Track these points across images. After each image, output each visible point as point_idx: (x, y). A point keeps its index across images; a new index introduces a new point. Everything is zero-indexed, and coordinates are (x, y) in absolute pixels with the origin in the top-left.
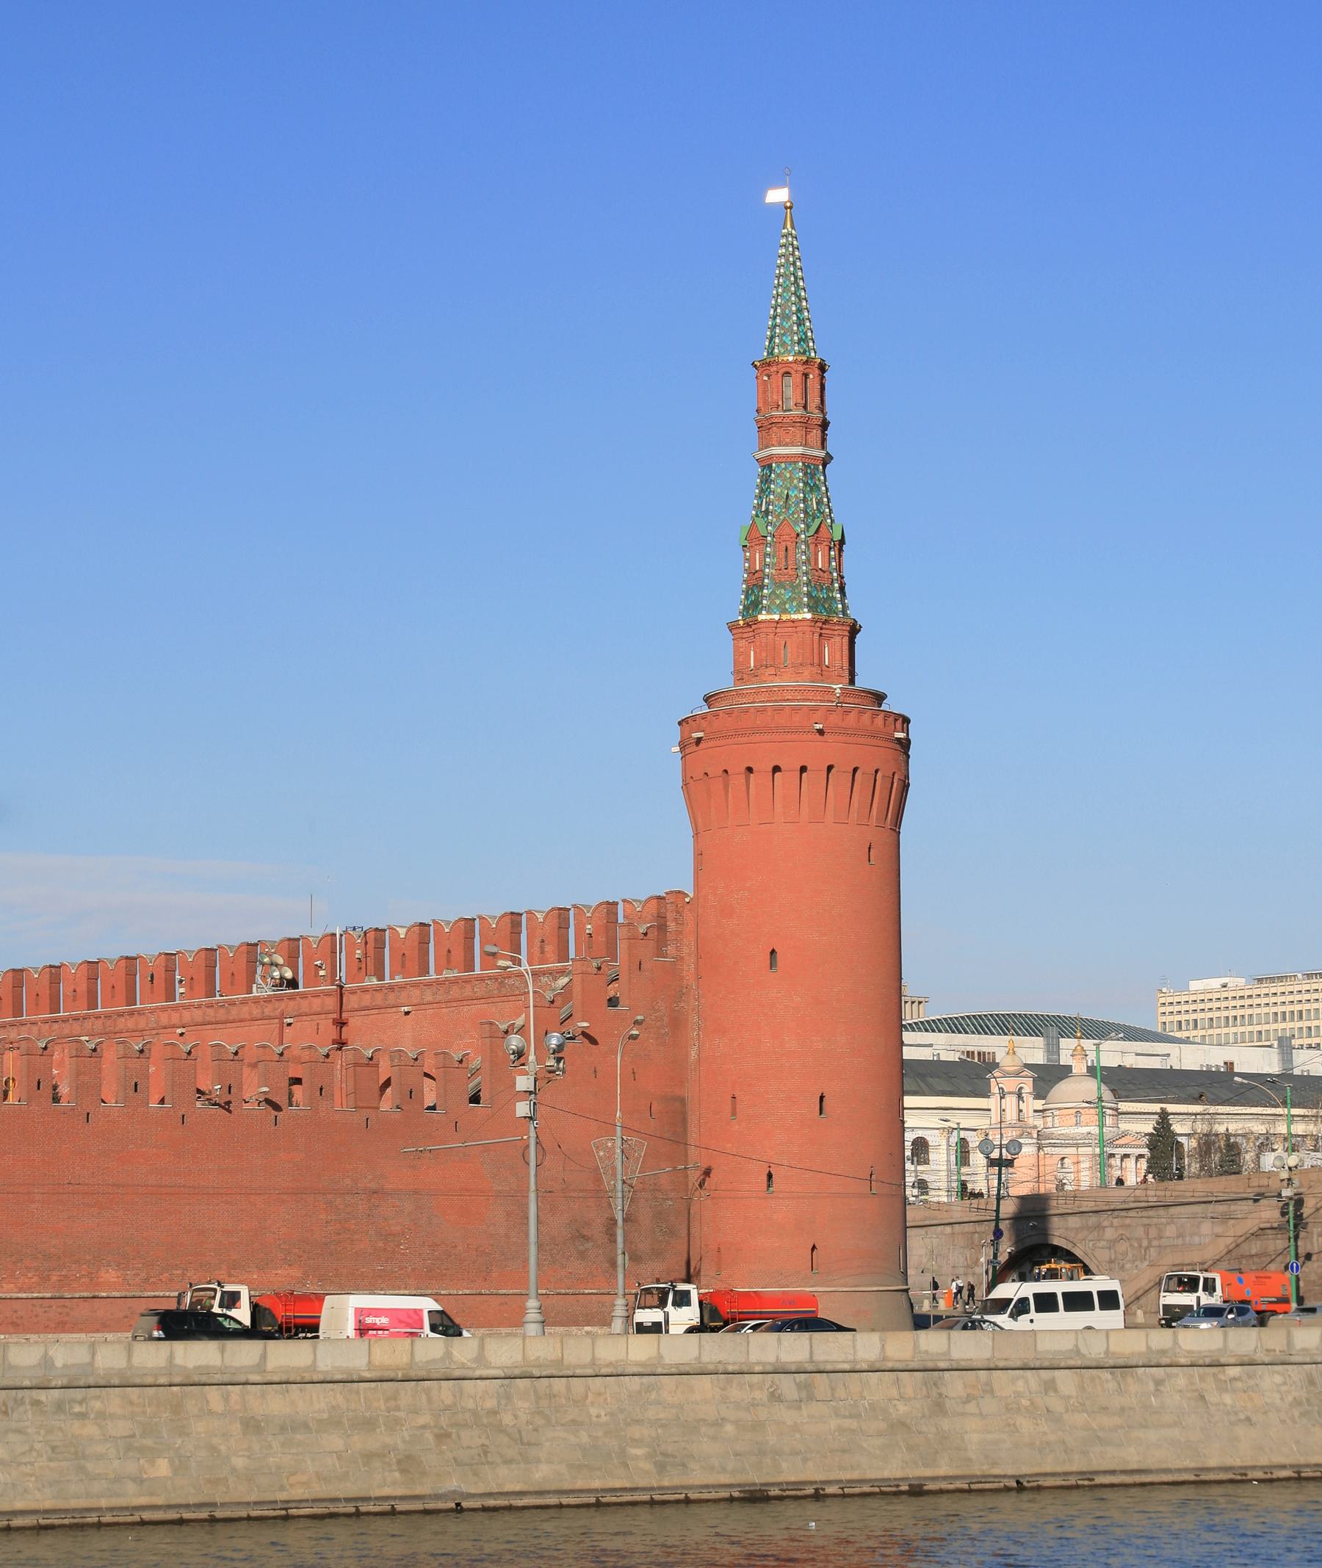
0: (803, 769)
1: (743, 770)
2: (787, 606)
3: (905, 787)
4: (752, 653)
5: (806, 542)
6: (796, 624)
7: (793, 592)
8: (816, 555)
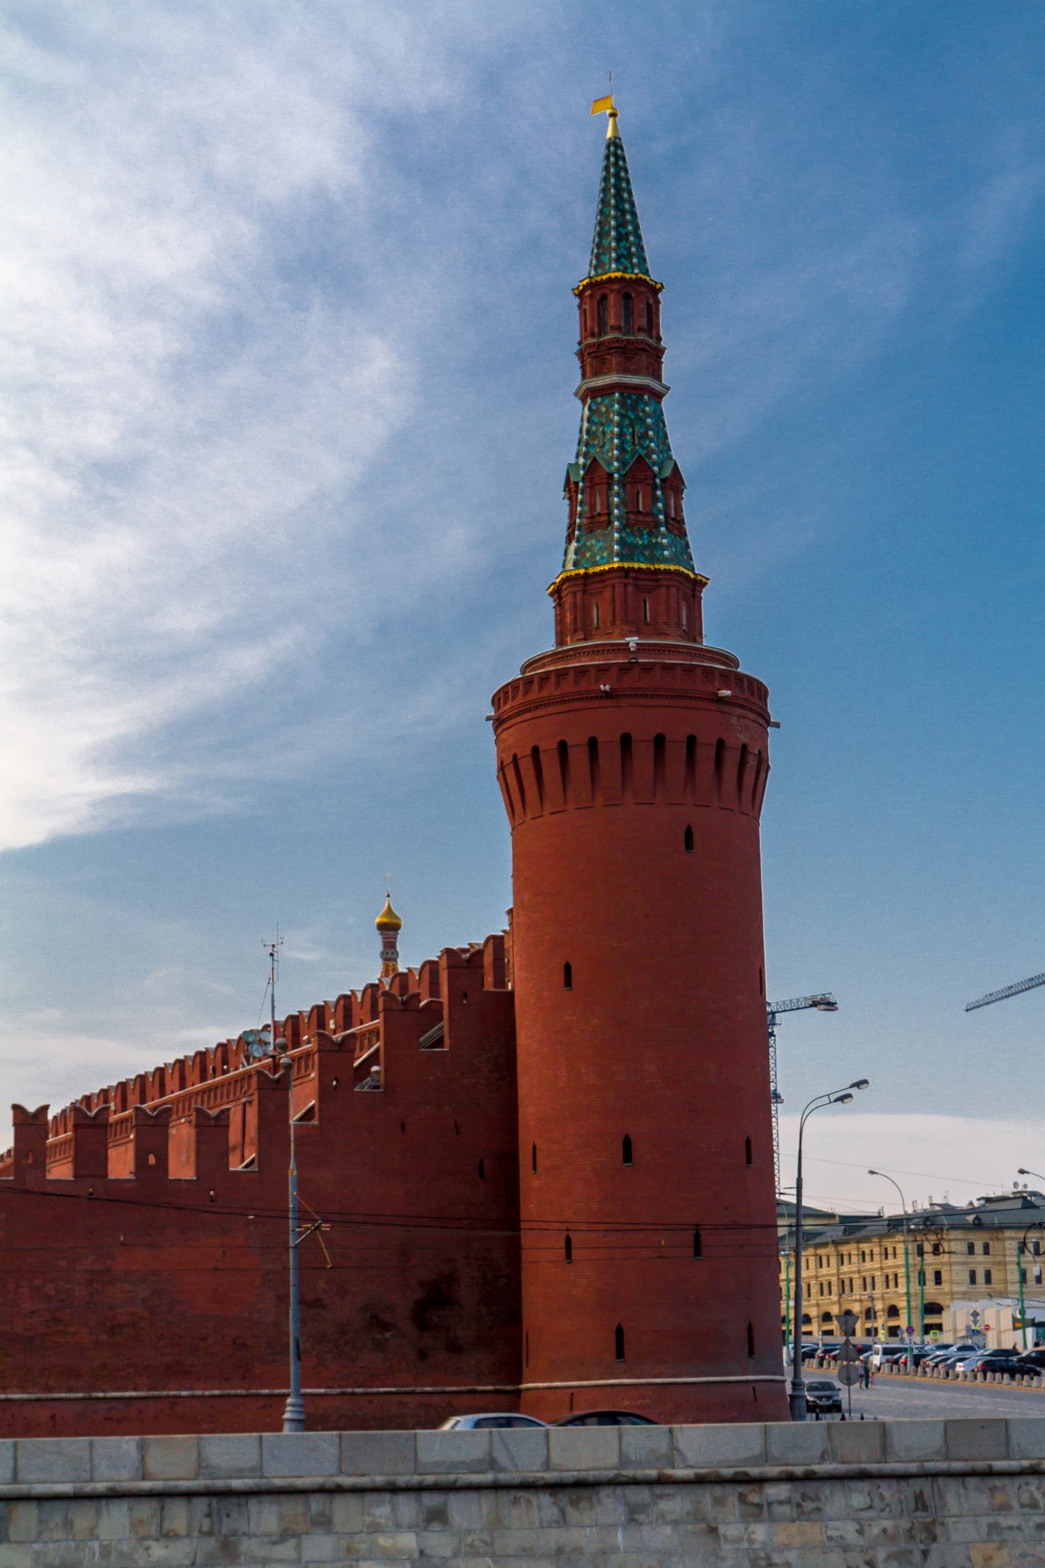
2: (598, 558)
5: (619, 483)
6: (605, 577)
7: (605, 541)
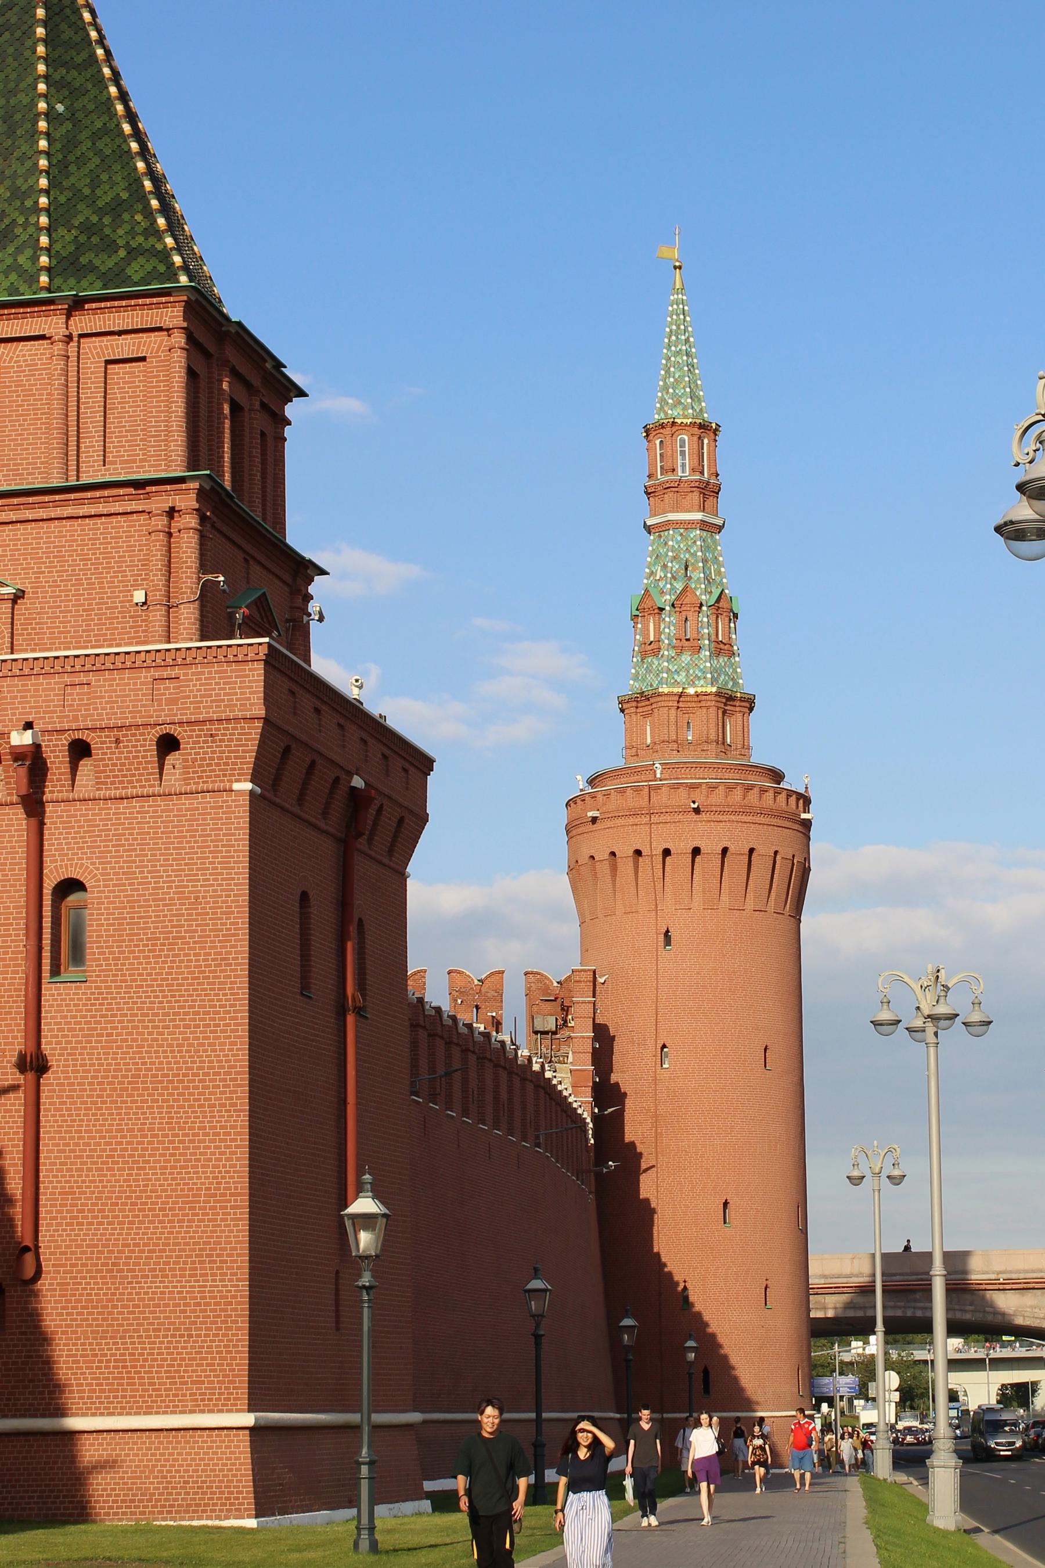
0: (667, 852)
1: (631, 853)
3: (806, 872)
4: (648, 728)
8: (717, 623)
